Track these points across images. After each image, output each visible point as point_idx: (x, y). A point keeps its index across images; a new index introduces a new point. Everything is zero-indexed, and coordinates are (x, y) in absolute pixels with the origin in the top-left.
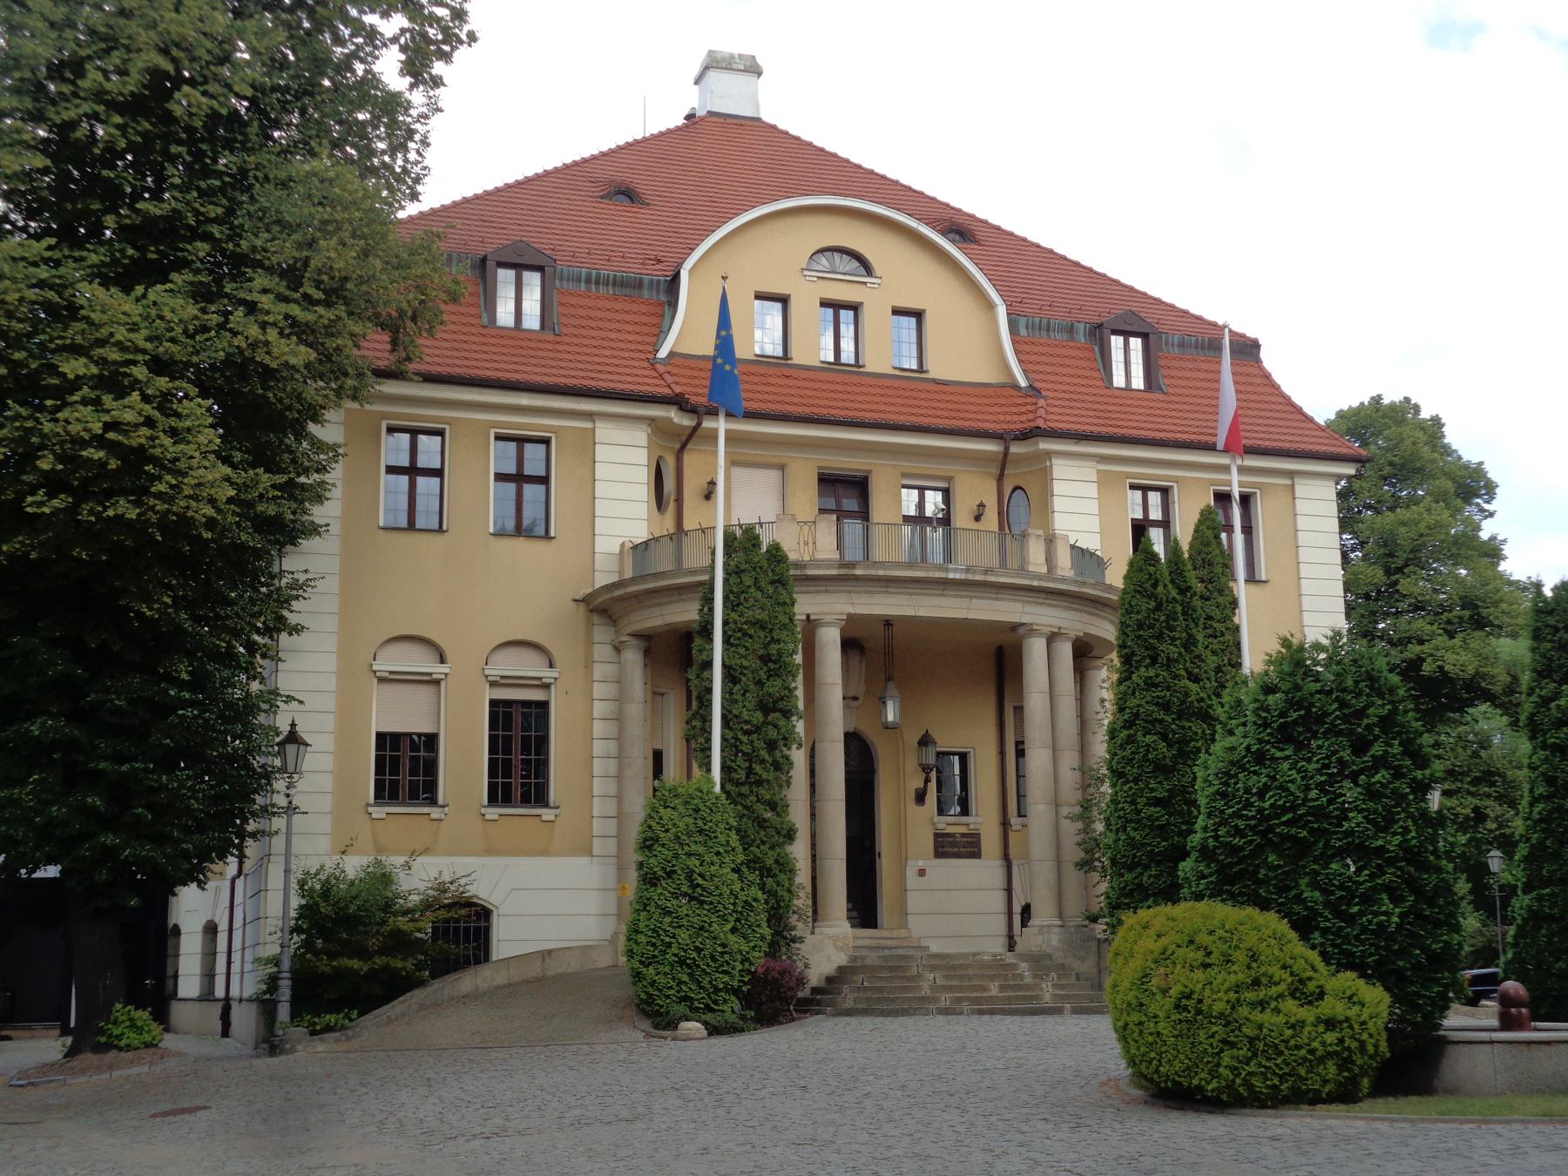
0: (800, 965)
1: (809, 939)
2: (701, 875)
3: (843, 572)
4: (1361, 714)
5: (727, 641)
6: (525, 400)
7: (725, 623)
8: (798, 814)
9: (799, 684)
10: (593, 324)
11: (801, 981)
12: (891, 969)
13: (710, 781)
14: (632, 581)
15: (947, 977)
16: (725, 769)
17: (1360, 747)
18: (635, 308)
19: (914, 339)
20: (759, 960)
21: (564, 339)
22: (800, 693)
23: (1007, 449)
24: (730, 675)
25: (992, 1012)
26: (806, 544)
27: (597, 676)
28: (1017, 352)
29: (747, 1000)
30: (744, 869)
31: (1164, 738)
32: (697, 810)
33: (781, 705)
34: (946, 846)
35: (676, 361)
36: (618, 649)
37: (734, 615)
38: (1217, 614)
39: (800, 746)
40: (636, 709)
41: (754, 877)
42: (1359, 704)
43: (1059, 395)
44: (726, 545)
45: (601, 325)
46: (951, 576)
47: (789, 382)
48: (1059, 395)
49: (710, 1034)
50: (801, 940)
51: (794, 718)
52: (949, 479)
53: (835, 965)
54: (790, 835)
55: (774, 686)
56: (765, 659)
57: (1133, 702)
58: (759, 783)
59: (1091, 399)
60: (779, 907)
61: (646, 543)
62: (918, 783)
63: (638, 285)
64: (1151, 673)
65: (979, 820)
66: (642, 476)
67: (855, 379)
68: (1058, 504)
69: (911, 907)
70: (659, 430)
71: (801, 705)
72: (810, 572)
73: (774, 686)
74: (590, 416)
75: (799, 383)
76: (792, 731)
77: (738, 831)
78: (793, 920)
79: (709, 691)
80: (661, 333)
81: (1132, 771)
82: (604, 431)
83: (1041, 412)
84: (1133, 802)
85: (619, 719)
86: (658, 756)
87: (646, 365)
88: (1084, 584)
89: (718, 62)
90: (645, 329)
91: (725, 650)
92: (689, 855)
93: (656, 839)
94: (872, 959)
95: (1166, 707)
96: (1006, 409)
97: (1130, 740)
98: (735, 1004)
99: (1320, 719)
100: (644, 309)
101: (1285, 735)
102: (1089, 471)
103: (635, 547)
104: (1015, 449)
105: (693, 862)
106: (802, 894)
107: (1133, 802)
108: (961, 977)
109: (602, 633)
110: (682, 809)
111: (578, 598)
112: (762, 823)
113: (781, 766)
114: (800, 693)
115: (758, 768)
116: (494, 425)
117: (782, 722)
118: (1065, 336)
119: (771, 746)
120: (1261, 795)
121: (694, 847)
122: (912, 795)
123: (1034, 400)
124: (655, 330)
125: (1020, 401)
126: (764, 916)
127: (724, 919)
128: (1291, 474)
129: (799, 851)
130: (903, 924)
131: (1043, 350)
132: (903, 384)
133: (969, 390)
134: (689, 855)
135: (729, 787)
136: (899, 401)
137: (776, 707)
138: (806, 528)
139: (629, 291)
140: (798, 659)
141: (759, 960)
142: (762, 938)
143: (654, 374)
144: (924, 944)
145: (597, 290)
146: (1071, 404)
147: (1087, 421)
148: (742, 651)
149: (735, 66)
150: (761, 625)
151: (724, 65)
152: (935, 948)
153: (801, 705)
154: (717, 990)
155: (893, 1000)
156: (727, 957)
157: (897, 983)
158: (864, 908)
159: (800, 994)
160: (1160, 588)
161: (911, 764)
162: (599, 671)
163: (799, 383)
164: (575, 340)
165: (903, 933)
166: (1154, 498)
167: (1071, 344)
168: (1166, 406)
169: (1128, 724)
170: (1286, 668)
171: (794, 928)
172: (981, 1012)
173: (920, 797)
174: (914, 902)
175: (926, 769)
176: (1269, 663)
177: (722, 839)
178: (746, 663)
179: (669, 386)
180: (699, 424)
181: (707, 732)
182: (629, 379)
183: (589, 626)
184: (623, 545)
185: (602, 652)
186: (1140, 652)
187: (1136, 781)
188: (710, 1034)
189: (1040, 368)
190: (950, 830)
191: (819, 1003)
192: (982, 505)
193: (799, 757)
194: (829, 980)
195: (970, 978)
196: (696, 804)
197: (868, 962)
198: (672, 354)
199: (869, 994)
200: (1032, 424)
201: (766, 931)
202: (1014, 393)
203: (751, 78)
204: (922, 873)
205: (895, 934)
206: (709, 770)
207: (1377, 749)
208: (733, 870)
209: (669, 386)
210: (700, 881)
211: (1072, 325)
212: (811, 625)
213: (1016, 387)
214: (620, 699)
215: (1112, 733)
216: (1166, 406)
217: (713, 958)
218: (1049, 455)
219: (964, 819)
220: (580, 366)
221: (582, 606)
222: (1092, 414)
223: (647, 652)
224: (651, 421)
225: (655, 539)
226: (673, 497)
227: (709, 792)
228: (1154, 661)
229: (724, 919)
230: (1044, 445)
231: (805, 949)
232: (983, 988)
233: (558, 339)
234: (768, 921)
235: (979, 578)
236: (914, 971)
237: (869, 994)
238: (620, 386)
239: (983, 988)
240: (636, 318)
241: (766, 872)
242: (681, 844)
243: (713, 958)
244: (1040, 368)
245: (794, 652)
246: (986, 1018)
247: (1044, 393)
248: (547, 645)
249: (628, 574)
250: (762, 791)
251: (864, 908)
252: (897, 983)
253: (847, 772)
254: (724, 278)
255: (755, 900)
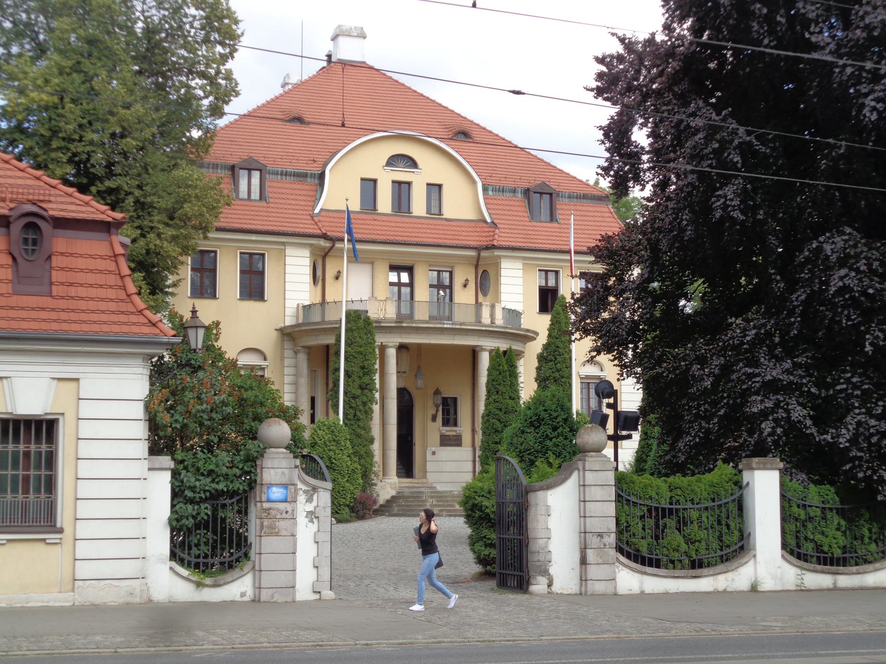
0: (375, 495)
1: (379, 484)
2: (334, 459)
3: (397, 325)
4: (556, 418)
5: (346, 359)
6: (254, 237)
7: (346, 352)
8: (376, 432)
9: (377, 377)
10: (284, 196)
11: (375, 502)
12: (414, 497)
13: (339, 420)
14: (303, 324)
15: (438, 501)
16: (345, 414)
17: (555, 429)
18: (304, 187)
19: (438, 198)
20: (358, 493)
21: (272, 205)
22: (377, 382)
23: (479, 254)
24: (348, 374)
25: (455, 516)
26: (381, 310)
27: (286, 364)
28: (488, 209)
29: (352, 509)
30: (352, 456)
31: (499, 421)
32: (333, 432)
33: (368, 387)
34: (448, 441)
35: (323, 213)
36: (296, 353)
37: (349, 349)
38: (561, 345)
39: (377, 404)
40: (304, 381)
41: (356, 459)
42: (555, 414)
43: (506, 227)
44: (347, 317)
45: (288, 197)
46: (445, 326)
47: (376, 223)
48: (506, 227)
49: (337, 522)
50: (376, 485)
51: (374, 392)
52: (452, 267)
53: (390, 496)
54: (372, 441)
55: (366, 379)
56: (363, 368)
57: (490, 407)
58: (359, 420)
59: (521, 228)
60: (366, 471)
61: (310, 305)
62: (433, 412)
63: (305, 175)
64: (496, 397)
65: (462, 429)
66: (307, 270)
67: (408, 220)
68: (503, 280)
69: (428, 470)
70: (314, 251)
71: (378, 386)
72: (382, 325)
73: (366, 379)
74: (284, 244)
75: (381, 223)
76: (373, 397)
77: (350, 440)
78: (373, 476)
79: (338, 380)
80: (317, 200)
81: (488, 432)
82: (289, 251)
83: (496, 237)
84: (488, 442)
85: (296, 384)
86: (313, 400)
87: (309, 218)
88: (506, 328)
89: (343, 32)
90: (309, 199)
91: (345, 364)
92: (330, 450)
93: (316, 443)
94: (407, 491)
95: (500, 410)
96: (479, 234)
97: (488, 421)
98: (347, 510)
99: (543, 420)
100: (308, 187)
101: (532, 424)
102: (519, 265)
103: (304, 307)
104: (484, 254)
105: (331, 453)
106: (376, 465)
107: (488, 442)
108: (444, 501)
109: (288, 345)
110: (327, 431)
111: (278, 328)
112: (359, 436)
113: (369, 413)
114: (377, 382)
115: (358, 413)
116: (240, 248)
117: (369, 394)
118: (511, 194)
119: (364, 404)
120: (522, 444)
121: (332, 447)
122: (430, 417)
123: (493, 230)
124: (313, 199)
125: (487, 230)
126: (360, 475)
127: (344, 476)
128: (284, 244)
129: (376, 447)
130: (425, 477)
131: (500, 202)
132: (431, 222)
133: (462, 224)
134: (330, 450)
135: (346, 421)
136: (428, 231)
137: (367, 387)
138: (381, 303)
139: (302, 179)
140: (377, 366)
141: (358, 493)
142: (359, 484)
143: (316, 227)
144: (434, 485)
145: (286, 179)
146: (511, 231)
147: (518, 240)
148: (353, 364)
149: (352, 34)
150: (361, 353)
151: (346, 33)
152: (440, 488)
153: (378, 386)
154: (340, 505)
155: (414, 510)
156: (344, 492)
157: (416, 503)
158: (406, 465)
159: (375, 507)
160: (501, 367)
161: (430, 403)
162: (287, 362)
163: (381, 223)
164: (276, 206)
165: (424, 480)
166: (551, 277)
167: (514, 199)
168: (558, 230)
169: (488, 415)
170: (535, 401)
171: (373, 480)
172: (451, 516)
173: (434, 419)
174: (430, 466)
175: (437, 406)
176: (530, 398)
177: (343, 443)
178: (354, 369)
179: (320, 229)
180: (333, 246)
181: (338, 398)
182: (302, 226)
183: (283, 341)
184: (298, 305)
185: (288, 353)
186: (493, 390)
187: (489, 435)
188: (337, 522)
189: (498, 212)
190: (447, 433)
191: (383, 511)
192: (467, 280)
193: (376, 408)
194: (388, 501)
195: (448, 501)
196: (332, 429)
197: (405, 494)
198: (322, 210)
199: (404, 508)
200: (491, 243)
201: (361, 481)
202: (484, 225)
203: (361, 40)
204: (434, 453)
205: (420, 481)
206: (338, 414)
207: (560, 430)
208: (348, 456)
209: (320, 229)
210: (334, 461)
211: (515, 189)
212: (383, 348)
213: (485, 222)
214: (296, 375)
215: (483, 417)
216: (558, 230)
217: (339, 492)
218: (499, 257)
219: (455, 428)
220: (279, 219)
221: (279, 332)
222: (521, 236)
223: (309, 354)
224: (311, 245)
225: (315, 305)
226: (321, 278)
227: (338, 424)
228: (497, 392)
229: (344, 476)
230: (497, 253)
231: (377, 488)
232: (453, 506)
233: (268, 205)
234: (362, 477)
235: (458, 327)
236: (424, 498)
237: (404, 508)
238: (298, 230)
239: (453, 506)
240: (304, 193)
241: (361, 457)
242: (326, 446)
243: (339, 492)
244: (498, 212)
245: (375, 363)
246: (452, 518)
247: (499, 226)
248: (263, 350)
249: (300, 321)
250: (360, 423)
251: (406, 465)
252: (416, 503)
253: (398, 406)
254: (347, 200)
255: (357, 469)
